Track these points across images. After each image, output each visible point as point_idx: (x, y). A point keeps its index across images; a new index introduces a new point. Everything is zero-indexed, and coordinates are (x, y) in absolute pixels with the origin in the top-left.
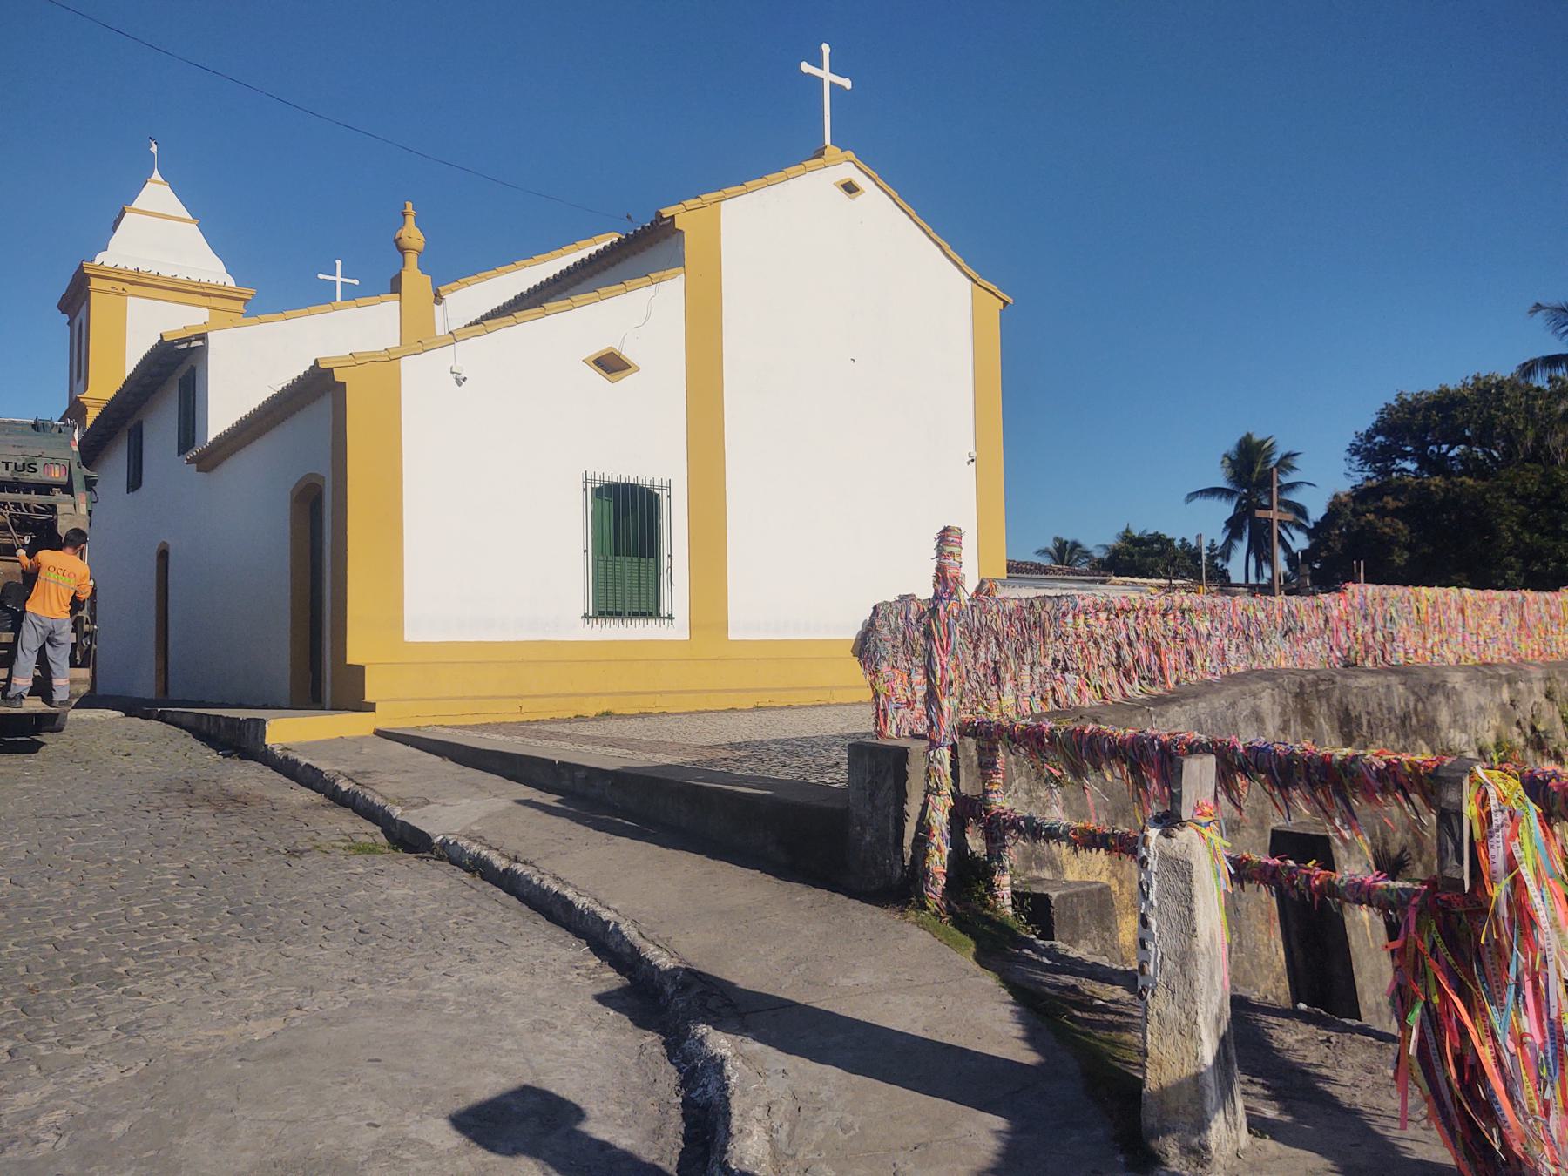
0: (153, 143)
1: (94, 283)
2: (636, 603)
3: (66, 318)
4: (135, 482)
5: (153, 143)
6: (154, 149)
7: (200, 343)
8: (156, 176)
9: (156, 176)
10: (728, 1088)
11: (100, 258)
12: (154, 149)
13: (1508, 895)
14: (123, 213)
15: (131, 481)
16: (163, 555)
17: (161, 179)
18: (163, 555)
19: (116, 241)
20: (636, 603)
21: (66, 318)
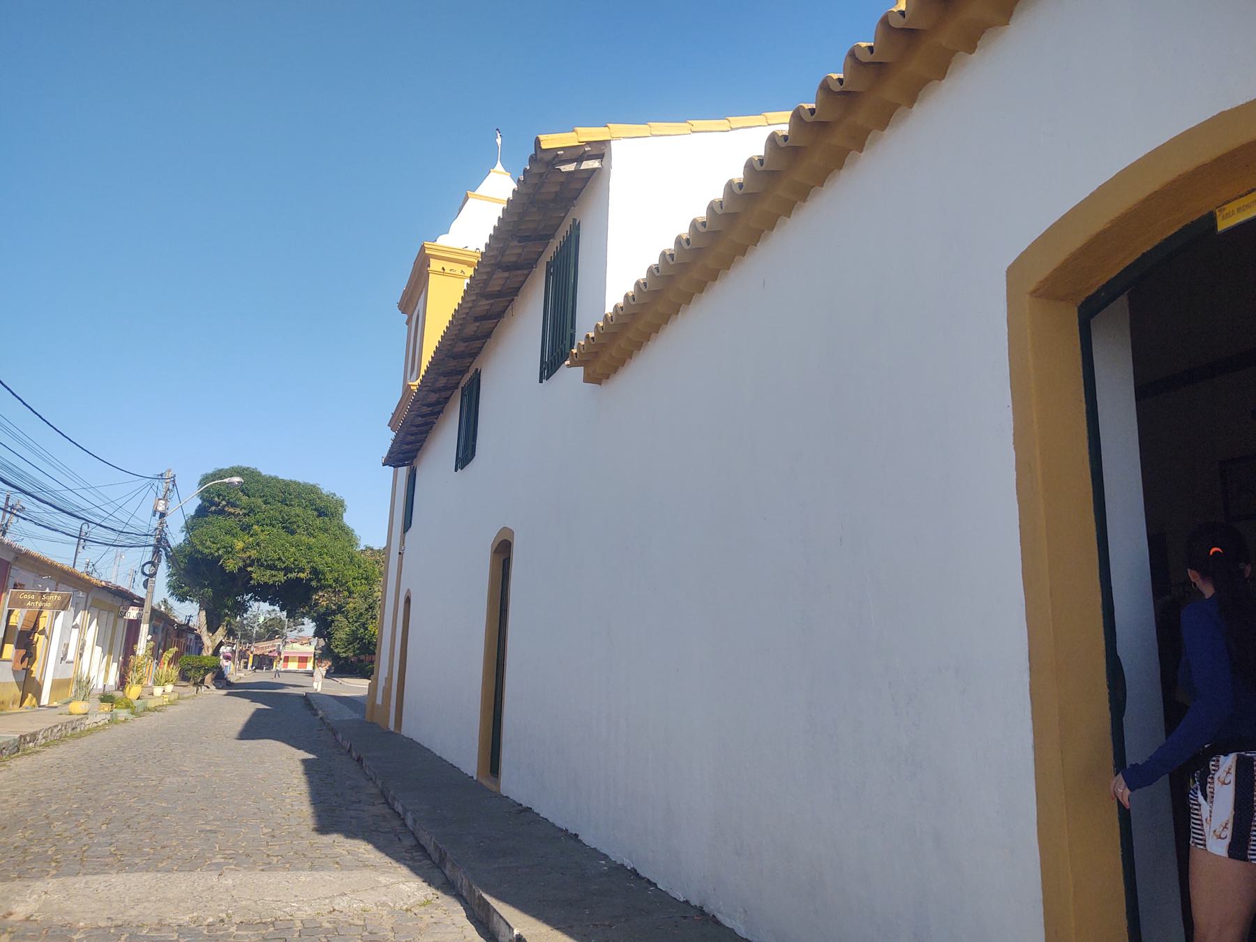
0: (499, 135)
1: (435, 265)
2: (1252, 852)
3: (406, 317)
4: (466, 454)
5: (499, 135)
6: (499, 141)
7: (594, 164)
8: (499, 167)
9: (499, 167)
10: (246, 611)
11: (443, 241)
12: (499, 141)
13: (89, 628)
14: (466, 198)
15: (460, 456)
16: (503, 551)
17: (503, 171)
18: (503, 551)
19: (455, 226)
20: (1252, 852)
21: (406, 317)
